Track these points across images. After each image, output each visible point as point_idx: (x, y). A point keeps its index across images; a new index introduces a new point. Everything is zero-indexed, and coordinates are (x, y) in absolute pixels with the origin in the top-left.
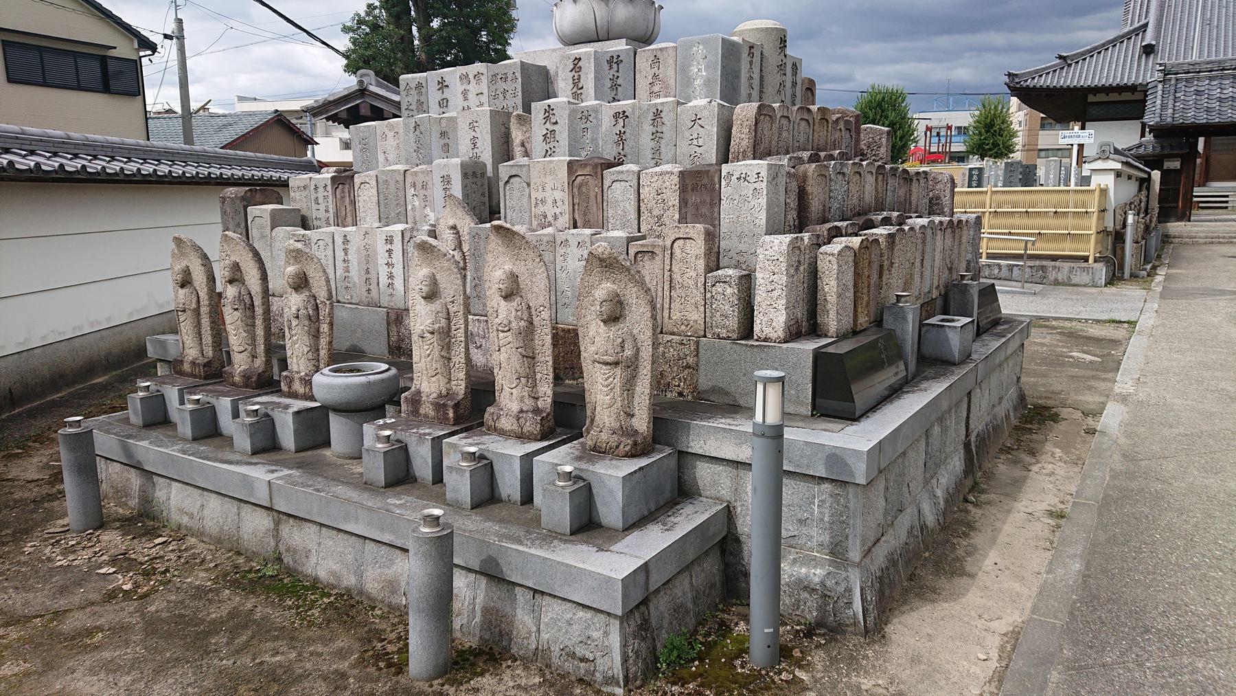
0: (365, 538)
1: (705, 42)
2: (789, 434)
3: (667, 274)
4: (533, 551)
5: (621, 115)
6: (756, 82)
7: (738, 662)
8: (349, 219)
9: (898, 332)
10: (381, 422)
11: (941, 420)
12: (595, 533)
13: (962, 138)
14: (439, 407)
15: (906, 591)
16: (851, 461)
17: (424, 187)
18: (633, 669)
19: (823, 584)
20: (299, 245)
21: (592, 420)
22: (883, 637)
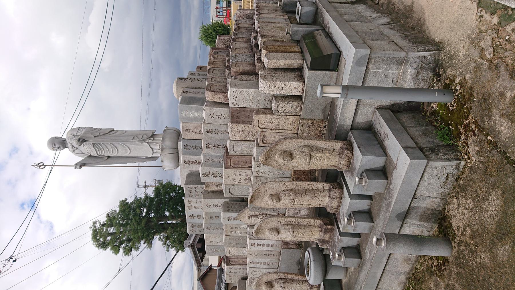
0: (384, 270)
1: (181, 111)
2: (345, 83)
3: (272, 131)
4: (395, 198)
5: (208, 146)
6: (198, 90)
7: (451, 108)
8: (244, 260)
9: (302, 33)
10: (331, 257)
11: (341, 15)
12: (387, 169)
13: (221, 2)
14: (326, 232)
15: (419, 32)
16: (360, 56)
17: (232, 228)
18: (453, 156)
19: (415, 69)
20: (254, 284)
21: (335, 166)
22: (441, 43)
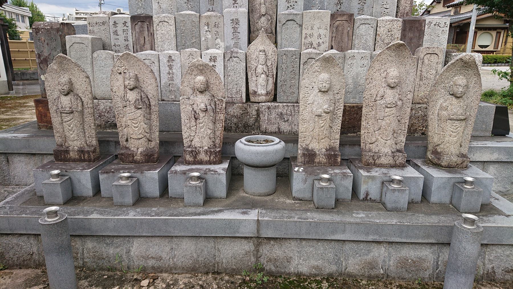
8: (148, 46)
